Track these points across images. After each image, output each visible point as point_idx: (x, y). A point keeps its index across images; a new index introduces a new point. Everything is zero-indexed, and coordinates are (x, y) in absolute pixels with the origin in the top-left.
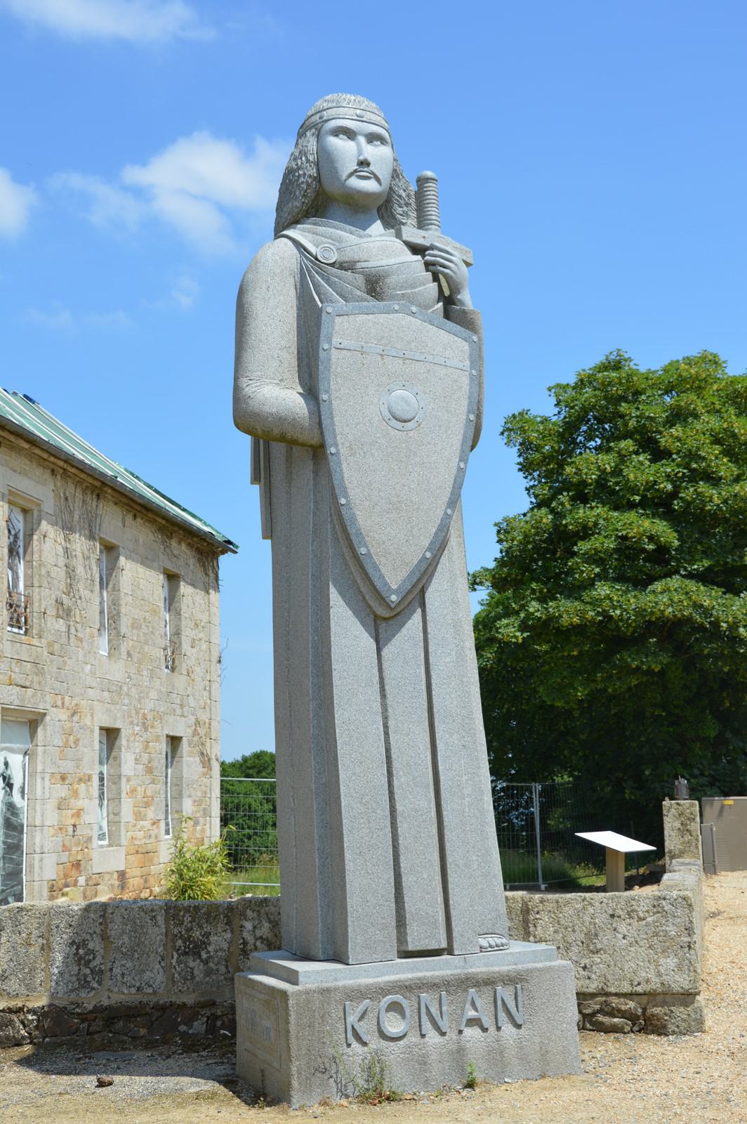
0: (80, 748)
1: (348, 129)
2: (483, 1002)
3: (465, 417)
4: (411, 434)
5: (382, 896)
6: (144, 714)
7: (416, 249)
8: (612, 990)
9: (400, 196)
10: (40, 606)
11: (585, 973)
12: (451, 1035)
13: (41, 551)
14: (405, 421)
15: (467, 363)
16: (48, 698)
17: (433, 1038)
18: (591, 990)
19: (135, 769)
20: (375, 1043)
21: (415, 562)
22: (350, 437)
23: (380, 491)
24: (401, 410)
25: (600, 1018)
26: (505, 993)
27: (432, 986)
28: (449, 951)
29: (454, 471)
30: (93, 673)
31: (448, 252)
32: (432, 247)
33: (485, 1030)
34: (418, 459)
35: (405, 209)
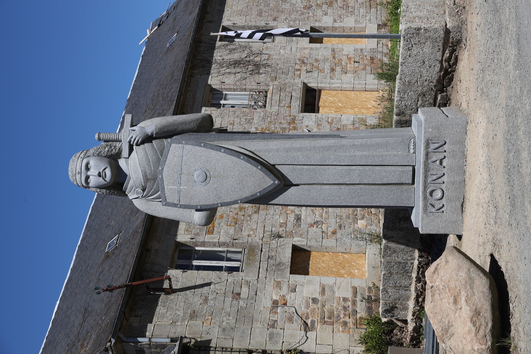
0: (319, 57)
2: (435, 157)
4: (212, 174)
6: (304, 8)
7: (131, 149)
8: (440, 58)
9: (108, 151)
10: (254, 85)
11: (432, 67)
12: (445, 171)
13: (229, 84)
15: (180, 145)
16: (296, 81)
17: (445, 179)
18: (439, 66)
19: (330, 16)
20: (444, 201)
21: (262, 173)
22: (214, 198)
23: (235, 188)
24: (202, 178)
25: (451, 63)
26: (433, 146)
27: (426, 177)
28: (414, 167)
30: (285, 48)
32: (130, 141)
33: (445, 157)
34: (222, 172)
35: (113, 148)
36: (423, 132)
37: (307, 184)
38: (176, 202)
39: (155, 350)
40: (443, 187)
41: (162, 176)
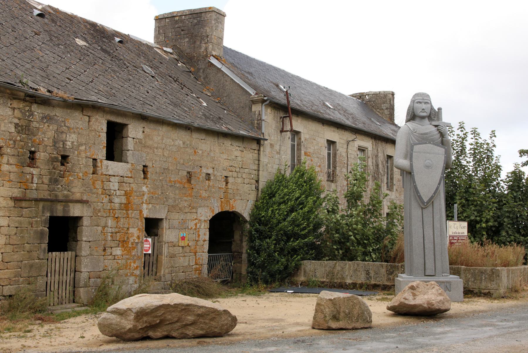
7: (436, 126)
26: (448, 285)
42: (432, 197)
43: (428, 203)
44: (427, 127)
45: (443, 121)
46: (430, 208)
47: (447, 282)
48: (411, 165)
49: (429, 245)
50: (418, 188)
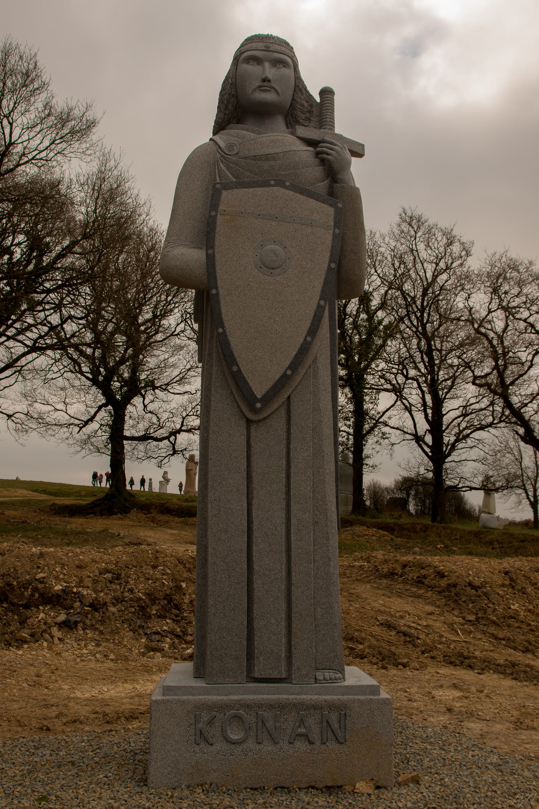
1: (256, 57)
3: (327, 266)
5: (236, 635)
7: (310, 143)
14: (273, 269)
21: (277, 377)
26: (334, 717)
27: (271, 706)
29: (314, 307)
31: (332, 143)
32: (323, 141)
33: (311, 743)
35: (308, 115)
36: (362, 697)
37: (249, 466)
38: (221, 207)
39: (45, 550)
40: (251, 744)
41: (273, 186)
42: (283, 381)
43: (268, 398)
44: (279, 140)
45: (337, 131)
46: (278, 424)
47: (332, 706)
48: (211, 260)
49: (268, 561)
50: (233, 345)
